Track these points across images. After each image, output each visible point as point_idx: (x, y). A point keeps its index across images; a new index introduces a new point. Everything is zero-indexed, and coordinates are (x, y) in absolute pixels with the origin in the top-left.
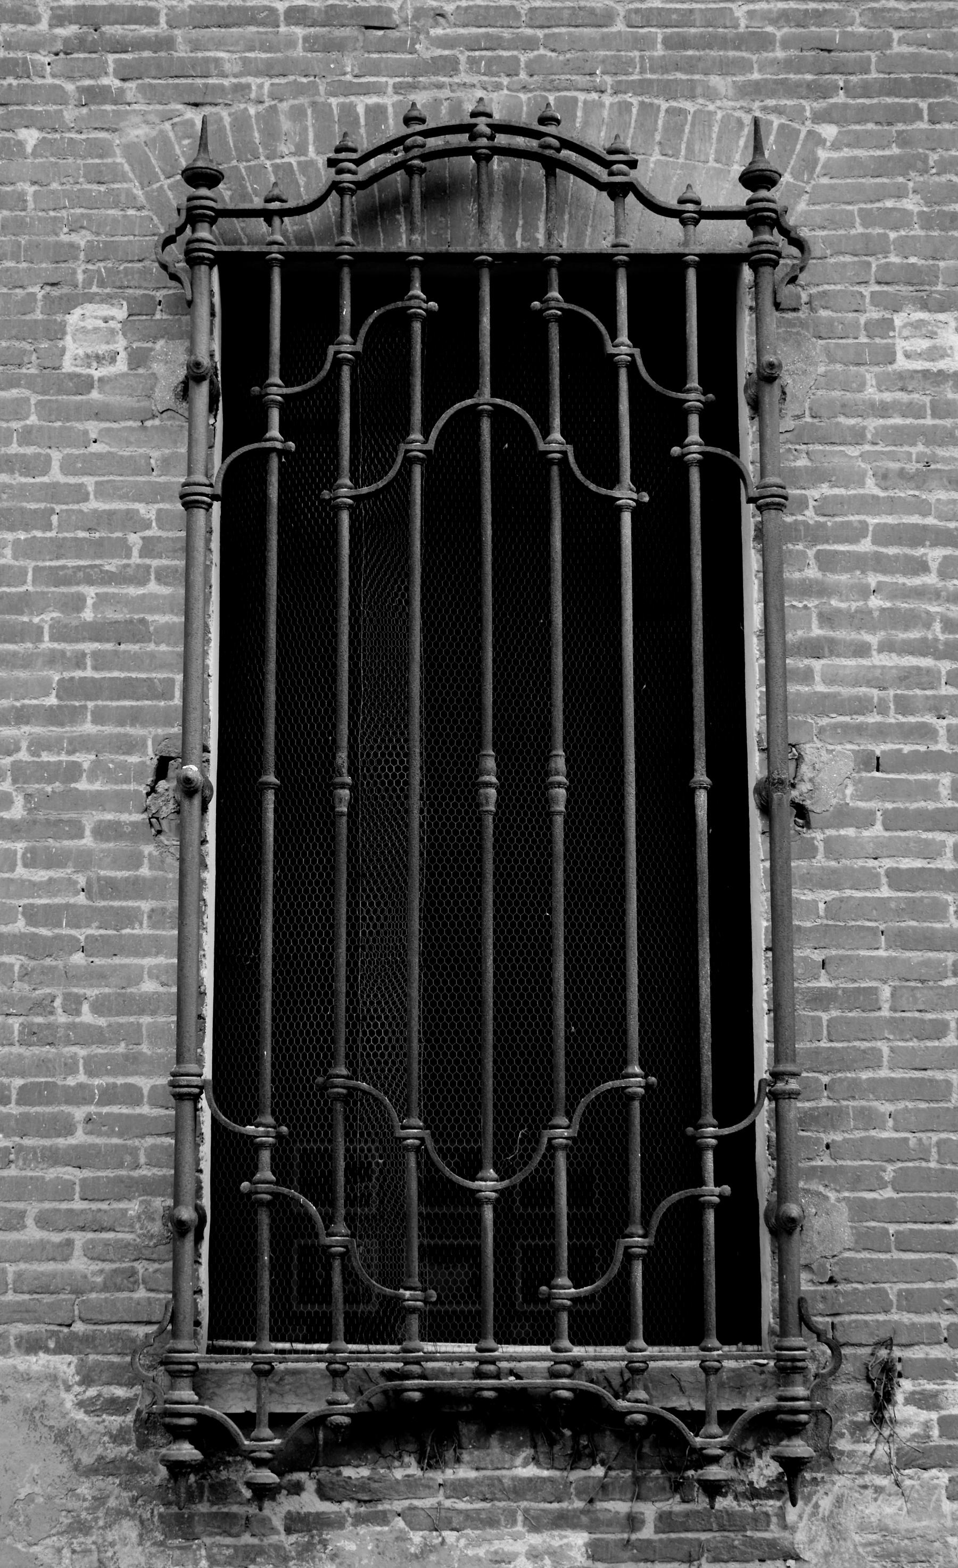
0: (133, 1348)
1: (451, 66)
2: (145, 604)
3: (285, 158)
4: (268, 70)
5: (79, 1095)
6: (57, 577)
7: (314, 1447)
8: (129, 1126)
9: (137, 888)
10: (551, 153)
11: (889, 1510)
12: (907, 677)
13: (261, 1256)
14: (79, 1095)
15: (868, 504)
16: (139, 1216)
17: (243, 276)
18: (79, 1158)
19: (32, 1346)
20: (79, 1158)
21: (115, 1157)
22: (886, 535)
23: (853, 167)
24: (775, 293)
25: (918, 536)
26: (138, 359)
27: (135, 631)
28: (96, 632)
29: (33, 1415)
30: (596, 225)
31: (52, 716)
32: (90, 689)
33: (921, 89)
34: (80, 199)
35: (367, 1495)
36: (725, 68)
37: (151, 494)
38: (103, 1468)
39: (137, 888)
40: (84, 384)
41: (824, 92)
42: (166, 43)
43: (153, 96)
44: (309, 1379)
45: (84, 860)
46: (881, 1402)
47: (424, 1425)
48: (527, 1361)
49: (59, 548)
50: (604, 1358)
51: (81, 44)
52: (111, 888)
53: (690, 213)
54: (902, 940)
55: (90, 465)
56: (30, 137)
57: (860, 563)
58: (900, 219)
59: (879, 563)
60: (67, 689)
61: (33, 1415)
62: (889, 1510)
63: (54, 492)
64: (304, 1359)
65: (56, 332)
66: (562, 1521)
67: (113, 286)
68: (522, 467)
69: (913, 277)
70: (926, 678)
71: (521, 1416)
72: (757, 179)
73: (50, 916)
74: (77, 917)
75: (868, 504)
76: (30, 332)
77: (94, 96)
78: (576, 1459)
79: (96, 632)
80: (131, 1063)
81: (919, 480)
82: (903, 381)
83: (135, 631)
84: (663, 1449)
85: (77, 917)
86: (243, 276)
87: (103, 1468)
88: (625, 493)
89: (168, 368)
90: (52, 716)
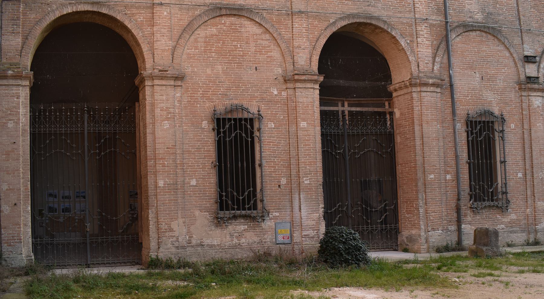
0: (212, 212)
1: (232, 99)
2: (210, 148)
3: (221, 108)
4: (218, 99)
5: (207, 191)
6: (203, 146)
7: (230, 218)
8: (211, 193)
9: (211, 173)
10: (243, 109)
11: (269, 223)
12: (270, 154)
13: (222, 205)
14: (207, 191)
15: (267, 139)
16: (213, 201)
17: (218, 120)
18: (207, 196)
19: (205, 212)
20: (207, 196)
21: (211, 196)
22: (268, 142)
23: (265, 109)
24: (514, 272)
25: (270, 142)
26: (208, 126)
27: (210, 151)
28: (207, 151)
29: (205, 217)
30: (246, 115)
31: (203, 158)
32: (206, 156)
33: (270, 102)
34: (203, 111)
35: (231, 223)
36: (255, 99)
37: (210, 139)
38: (211, 222)
39: (211, 173)
40: (204, 129)
41: (262, 102)
42: (209, 97)
43: (209, 102)
44: (227, 214)
45: (207, 171)
46: (268, 215)
47: (235, 217)
48: (243, 212)
49: (203, 143)
50: (249, 212)
51: (202, 97)
52: (209, 173)
53: (253, 114)
54: (269, 177)
55: (205, 136)
56: (198, 105)
57: (266, 144)
58: (268, 114)
59: (267, 145)
60: (204, 156)
61: (205, 217)
62: (269, 223)
63: (202, 138)
64: (227, 212)
65: (202, 124)
66: (245, 225)
67: (206, 120)
68: (241, 136)
69: (269, 119)
70: (271, 154)
71: (245, 217)
72: (259, 111)
73: (204, 176)
74: (206, 176)
75: (267, 139)
76: (199, 124)
77: (204, 102)
78: (246, 220)
79: (207, 151)
80: (211, 188)
81: (270, 137)
82: (269, 128)
83: (210, 151)
84: (253, 219)
85: (206, 176)
86: (218, 120)
87: (211, 222)
88: (249, 140)
89: (211, 127)
90: (203, 158)
